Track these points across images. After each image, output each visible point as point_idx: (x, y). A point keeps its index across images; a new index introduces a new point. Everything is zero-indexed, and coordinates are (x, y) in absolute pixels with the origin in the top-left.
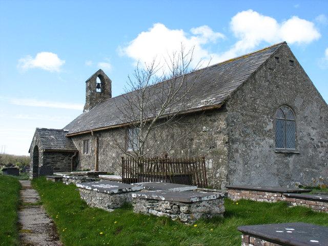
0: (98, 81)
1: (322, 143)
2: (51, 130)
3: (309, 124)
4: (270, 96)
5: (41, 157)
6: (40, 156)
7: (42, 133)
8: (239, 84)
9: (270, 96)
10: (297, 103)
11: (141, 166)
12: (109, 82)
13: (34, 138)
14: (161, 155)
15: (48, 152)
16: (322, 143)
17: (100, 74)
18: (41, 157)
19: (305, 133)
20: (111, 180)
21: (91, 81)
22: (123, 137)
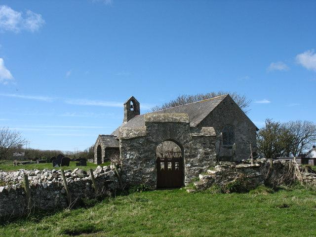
0: (132, 103)
1: (249, 142)
2: (107, 136)
3: (241, 133)
4: (220, 122)
5: (103, 152)
6: (102, 151)
7: (102, 137)
8: (204, 117)
9: (220, 122)
10: (235, 123)
11: (162, 154)
12: (138, 104)
13: (97, 140)
14: (170, 150)
15: (108, 149)
16: (249, 142)
17: (133, 99)
18: (103, 152)
19: (239, 138)
20: (76, 233)
21: (128, 103)
22: (31, 185)
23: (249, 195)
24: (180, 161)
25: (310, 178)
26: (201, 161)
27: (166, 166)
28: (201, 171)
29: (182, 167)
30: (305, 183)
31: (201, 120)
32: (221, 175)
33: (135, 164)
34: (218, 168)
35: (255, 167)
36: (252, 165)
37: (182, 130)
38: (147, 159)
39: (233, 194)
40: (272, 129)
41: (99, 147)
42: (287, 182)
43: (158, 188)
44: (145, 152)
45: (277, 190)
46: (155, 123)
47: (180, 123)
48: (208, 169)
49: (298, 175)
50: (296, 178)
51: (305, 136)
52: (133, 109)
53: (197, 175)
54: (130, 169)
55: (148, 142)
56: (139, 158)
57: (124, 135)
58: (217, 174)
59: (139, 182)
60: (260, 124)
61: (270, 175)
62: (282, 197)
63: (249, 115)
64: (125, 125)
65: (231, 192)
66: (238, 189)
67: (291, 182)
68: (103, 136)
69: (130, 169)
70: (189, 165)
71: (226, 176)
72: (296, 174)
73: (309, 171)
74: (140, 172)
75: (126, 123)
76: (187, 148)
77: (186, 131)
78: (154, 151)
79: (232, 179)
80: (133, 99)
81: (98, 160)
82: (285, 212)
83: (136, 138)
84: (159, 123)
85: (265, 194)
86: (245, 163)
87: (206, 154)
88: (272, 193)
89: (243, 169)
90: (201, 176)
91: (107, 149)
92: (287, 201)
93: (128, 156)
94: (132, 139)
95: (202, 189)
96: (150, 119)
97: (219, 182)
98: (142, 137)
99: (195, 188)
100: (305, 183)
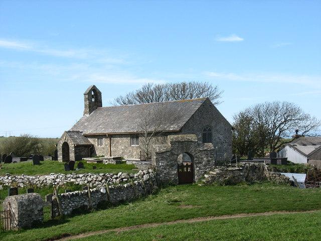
6: (70, 148)
8: (187, 120)
10: (213, 124)
12: (100, 93)
17: (94, 89)
23: (236, 186)
24: (192, 166)
25: (274, 175)
26: (205, 166)
27: (187, 169)
28: (205, 173)
29: (193, 170)
30: (271, 179)
31: (184, 123)
32: (220, 175)
33: (165, 169)
34: (217, 171)
35: (239, 170)
36: (237, 168)
37: (192, 147)
38: (172, 166)
39: (227, 186)
40: (245, 120)
41: (66, 145)
42: (259, 178)
43: (179, 184)
44: (171, 160)
45: (253, 183)
46: (176, 142)
47: (192, 141)
48: (210, 171)
49: (267, 174)
50: (265, 176)
51: (283, 120)
52: (94, 99)
53: (203, 175)
54: (162, 172)
55: (173, 154)
56: (167, 165)
57: (158, 151)
58: (217, 174)
59: (168, 180)
60: (232, 121)
61: (248, 174)
62: (256, 187)
63: (218, 107)
64: (88, 118)
65: (226, 185)
66: (228, 183)
67: (263, 179)
68: (69, 132)
69: (162, 172)
70: (198, 169)
71: (222, 175)
72: (265, 172)
73: (274, 171)
74: (168, 173)
75: (88, 115)
76: (197, 157)
77: (196, 147)
78: (176, 160)
79: (226, 177)
80: (94, 89)
81: (63, 158)
82: (257, 193)
83: (165, 152)
84: (179, 142)
85: (246, 186)
86: (233, 167)
87: (209, 161)
88: (250, 185)
89: (232, 171)
90: (206, 176)
91: (77, 147)
92: (258, 189)
93: (160, 164)
94: (162, 153)
95: (208, 183)
96: (173, 139)
97: (219, 179)
98: (169, 151)
99: (204, 183)
100: (271, 179)
